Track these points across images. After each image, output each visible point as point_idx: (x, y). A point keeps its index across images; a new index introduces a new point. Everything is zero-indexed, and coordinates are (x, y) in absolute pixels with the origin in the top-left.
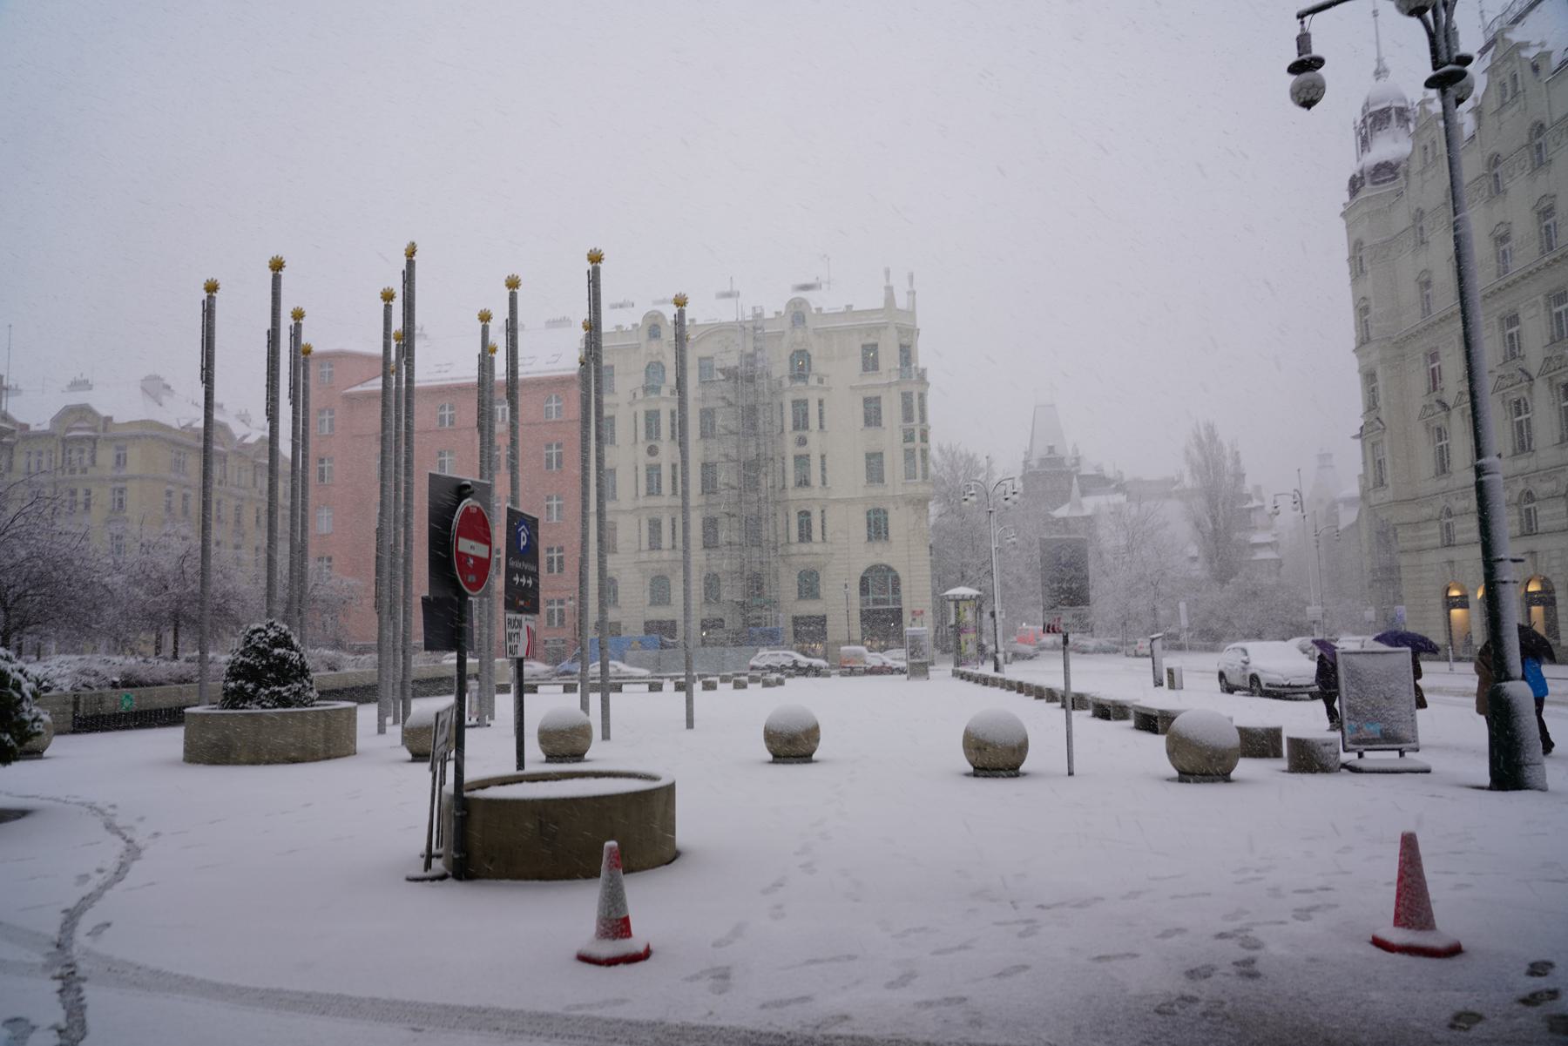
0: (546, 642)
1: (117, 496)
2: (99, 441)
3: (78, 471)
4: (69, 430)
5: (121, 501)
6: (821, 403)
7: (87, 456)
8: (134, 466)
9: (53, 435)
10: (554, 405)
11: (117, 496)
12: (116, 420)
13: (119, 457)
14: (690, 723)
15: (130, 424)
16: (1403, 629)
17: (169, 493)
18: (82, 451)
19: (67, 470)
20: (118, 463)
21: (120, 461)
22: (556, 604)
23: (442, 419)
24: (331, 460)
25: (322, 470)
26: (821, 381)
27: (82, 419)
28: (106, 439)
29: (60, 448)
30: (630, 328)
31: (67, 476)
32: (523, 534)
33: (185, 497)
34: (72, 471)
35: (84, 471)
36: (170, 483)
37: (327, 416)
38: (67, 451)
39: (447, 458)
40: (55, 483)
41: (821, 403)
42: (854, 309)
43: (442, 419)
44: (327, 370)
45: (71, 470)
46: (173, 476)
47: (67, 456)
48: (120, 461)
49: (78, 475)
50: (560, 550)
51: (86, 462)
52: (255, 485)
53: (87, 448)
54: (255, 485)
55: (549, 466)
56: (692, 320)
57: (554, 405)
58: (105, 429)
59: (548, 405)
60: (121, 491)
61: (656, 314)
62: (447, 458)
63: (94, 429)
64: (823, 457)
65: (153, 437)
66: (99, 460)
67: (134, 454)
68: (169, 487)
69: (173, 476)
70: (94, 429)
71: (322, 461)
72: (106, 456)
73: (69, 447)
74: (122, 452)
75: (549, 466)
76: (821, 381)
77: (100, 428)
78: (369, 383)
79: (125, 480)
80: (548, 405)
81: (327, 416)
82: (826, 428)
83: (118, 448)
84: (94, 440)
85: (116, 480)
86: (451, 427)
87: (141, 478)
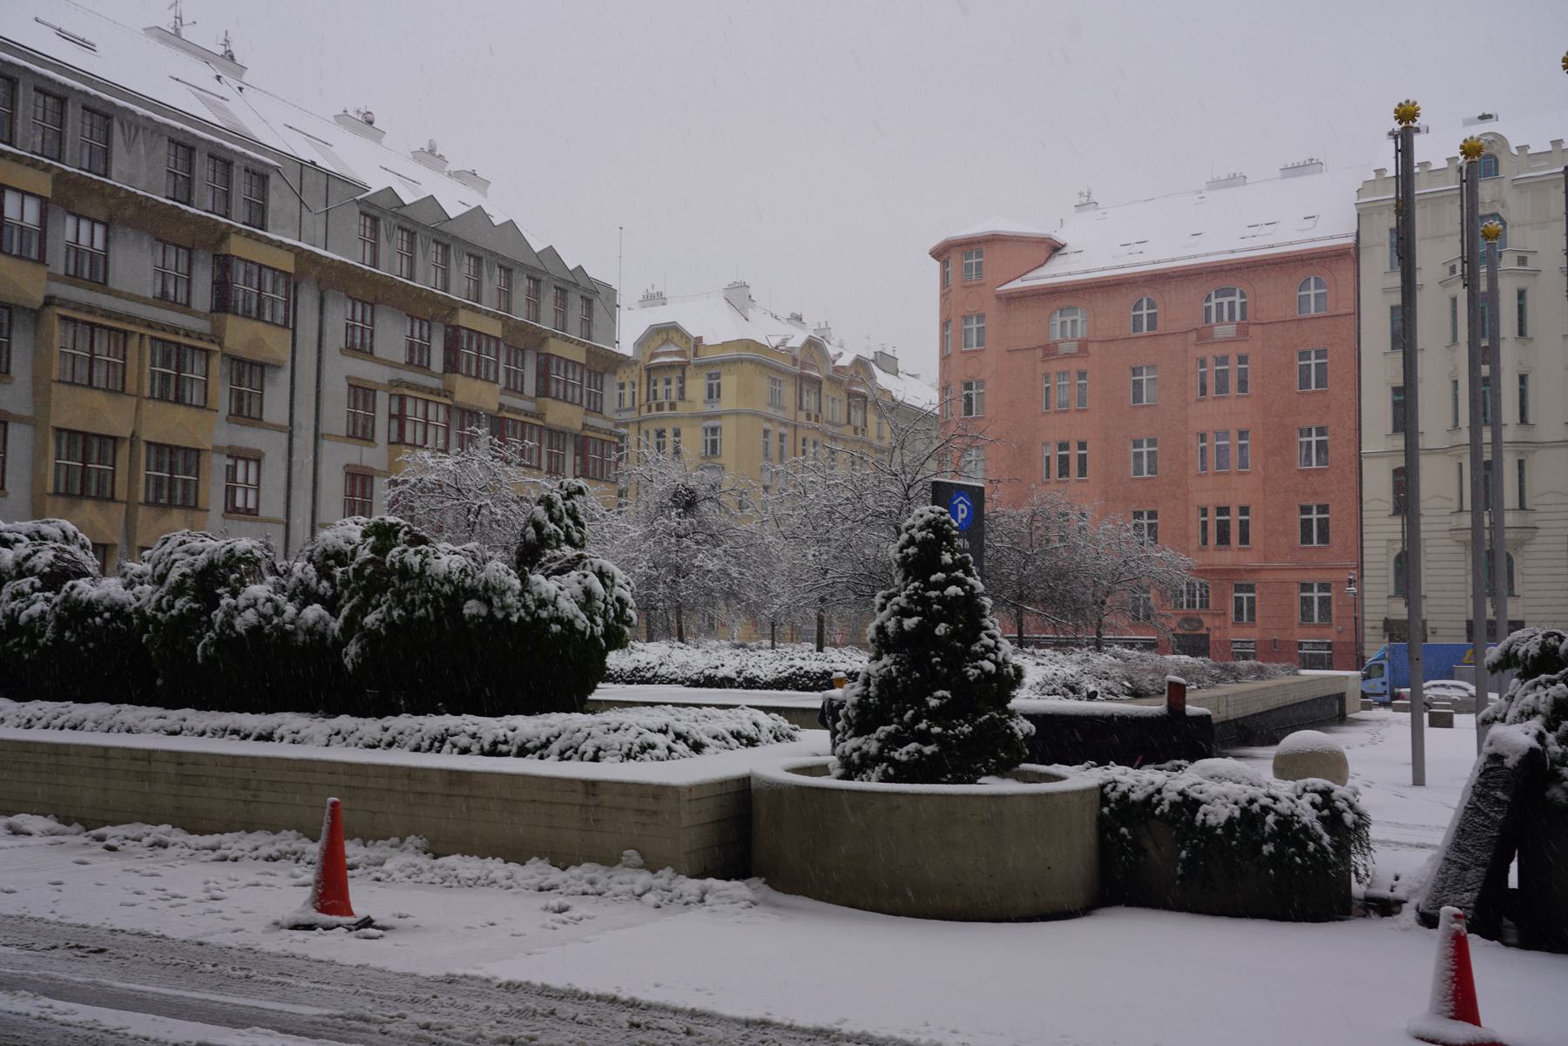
0: (1300, 645)
1: (709, 438)
2: (688, 369)
3: (667, 406)
4: (653, 356)
5: (714, 442)
6: (1521, 294)
7: (674, 386)
8: (728, 401)
9: (636, 362)
10: (1312, 292)
11: (709, 438)
12: (708, 340)
13: (710, 387)
14: (1419, 780)
15: (725, 345)
16: (1292, 697)
17: (766, 433)
18: (668, 382)
19: (654, 407)
20: (710, 396)
21: (713, 393)
22: (1316, 589)
23: (1137, 321)
24: (981, 383)
25: (969, 398)
26: (1522, 261)
27: (666, 341)
28: (700, 366)
29: (644, 380)
30: (1445, 164)
31: (654, 412)
32: (961, 506)
33: (782, 437)
34: (660, 407)
35: (673, 406)
36: (769, 420)
37: (974, 325)
38: (652, 383)
39: (1144, 378)
40: (639, 422)
41: (1521, 294)
42: (1530, 151)
43: (1137, 321)
44: (974, 261)
45: (658, 405)
46: (771, 411)
47: (652, 388)
48: (713, 393)
49: (666, 411)
50: (1323, 509)
51: (674, 394)
52: (849, 422)
53: (674, 376)
54: (849, 422)
55: (1305, 383)
56: (1425, 164)
57: (1312, 292)
58: (695, 355)
59: (1303, 293)
60: (714, 430)
61: (1491, 138)
62: (1144, 378)
63: (681, 353)
64: (1523, 379)
65: (752, 361)
66: (689, 394)
67: (729, 383)
68: (767, 426)
69: (771, 411)
70: (681, 353)
71: (968, 386)
72: (696, 387)
73: (653, 378)
74: (715, 382)
75: (1305, 383)
76: (1522, 261)
77: (690, 353)
78: (1029, 275)
79: (718, 416)
80: (1303, 293)
81: (974, 325)
82: (1529, 333)
83: (710, 376)
84: (682, 367)
85: (708, 417)
86: (1152, 332)
87: (737, 413)
